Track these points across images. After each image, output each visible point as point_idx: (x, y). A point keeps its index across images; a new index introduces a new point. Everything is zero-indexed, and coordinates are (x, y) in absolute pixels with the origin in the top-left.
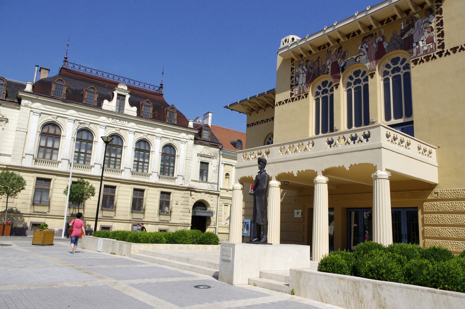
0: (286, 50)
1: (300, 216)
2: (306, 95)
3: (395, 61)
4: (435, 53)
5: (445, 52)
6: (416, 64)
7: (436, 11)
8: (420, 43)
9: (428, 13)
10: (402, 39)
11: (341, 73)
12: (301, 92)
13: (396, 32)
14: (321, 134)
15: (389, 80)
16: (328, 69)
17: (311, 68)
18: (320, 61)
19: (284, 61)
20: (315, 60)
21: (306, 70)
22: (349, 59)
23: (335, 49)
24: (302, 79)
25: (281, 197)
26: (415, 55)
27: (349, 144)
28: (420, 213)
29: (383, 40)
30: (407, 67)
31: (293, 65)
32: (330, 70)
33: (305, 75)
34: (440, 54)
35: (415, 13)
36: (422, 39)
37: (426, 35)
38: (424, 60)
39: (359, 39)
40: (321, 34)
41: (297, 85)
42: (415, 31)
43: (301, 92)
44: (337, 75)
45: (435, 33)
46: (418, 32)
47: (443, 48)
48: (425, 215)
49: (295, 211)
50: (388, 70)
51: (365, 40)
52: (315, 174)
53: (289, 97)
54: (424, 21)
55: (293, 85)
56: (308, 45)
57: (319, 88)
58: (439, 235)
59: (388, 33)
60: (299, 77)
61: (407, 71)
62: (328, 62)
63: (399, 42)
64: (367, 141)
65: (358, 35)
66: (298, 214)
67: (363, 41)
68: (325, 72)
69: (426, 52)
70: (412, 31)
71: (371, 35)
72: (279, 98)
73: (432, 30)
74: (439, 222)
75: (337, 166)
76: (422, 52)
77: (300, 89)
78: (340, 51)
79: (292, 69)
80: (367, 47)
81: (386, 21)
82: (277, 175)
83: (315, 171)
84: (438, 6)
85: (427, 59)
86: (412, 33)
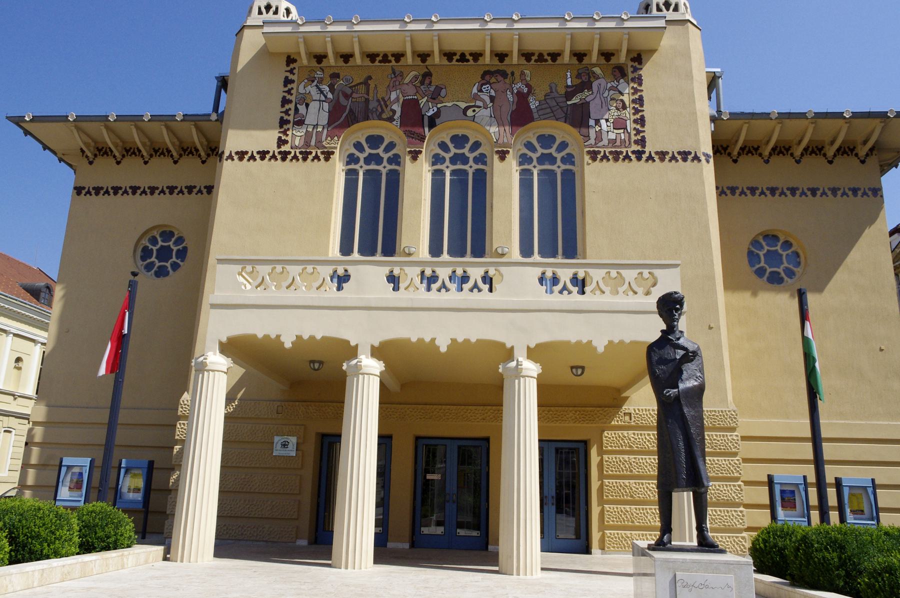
0: (289, 29)
1: (291, 452)
2: (328, 155)
3: (375, 141)
4: (630, 150)
5: (647, 154)
6: (594, 159)
7: (631, 76)
8: (603, 122)
9: (618, 74)
10: (569, 103)
11: (426, 129)
12: (313, 143)
13: (556, 86)
14: (356, 255)
15: (358, 174)
16: (394, 112)
17: (347, 96)
18: (372, 86)
19: (265, 53)
20: (357, 80)
21: (330, 96)
22: (449, 104)
23: (413, 73)
24: (317, 114)
25: (229, 399)
26: (592, 141)
27: (480, 290)
28: (594, 452)
29: (529, 92)
30: (396, 160)
31: (291, 71)
32: (398, 114)
33: (326, 106)
34: (639, 155)
35: (595, 65)
36: (606, 117)
37: (613, 113)
38: (279, 157)
39: (473, 71)
40: (396, 27)
41: (300, 123)
42: (592, 97)
43: (313, 143)
44: (418, 130)
45: (628, 114)
46: (598, 101)
47: (644, 146)
48: (605, 457)
49: (276, 439)
50: (357, 153)
51: (487, 78)
52: (352, 352)
53: (272, 147)
54: (609, 85)
55: (288, 122)
56: (301, 40)
57: (358, 146)
58: (632, 496)
59: (542, 84)
60: (307, 105)
61: (394, 167)
62: (393, 96)
63: (561, 107)
64: (339, 288)
65: (471, 62)
66: (286, 446)
67: (483, 77)
68: (384, 116)
69: (612, 142)
70: (586, 95)
71: (504, 74)
72: (234, 140)
73: (624, 107)
74: (631, 471)
75: (414, 339)
76: (605, 142)
77: (308, 135)
78: (427, 81)
79: (287, 81)
80: (493, 93)
81: (542, 58)
82: (224, 340)
83: (353, 344)
84: (635, 70)
85: (616, 156)
86: (588, 99)
